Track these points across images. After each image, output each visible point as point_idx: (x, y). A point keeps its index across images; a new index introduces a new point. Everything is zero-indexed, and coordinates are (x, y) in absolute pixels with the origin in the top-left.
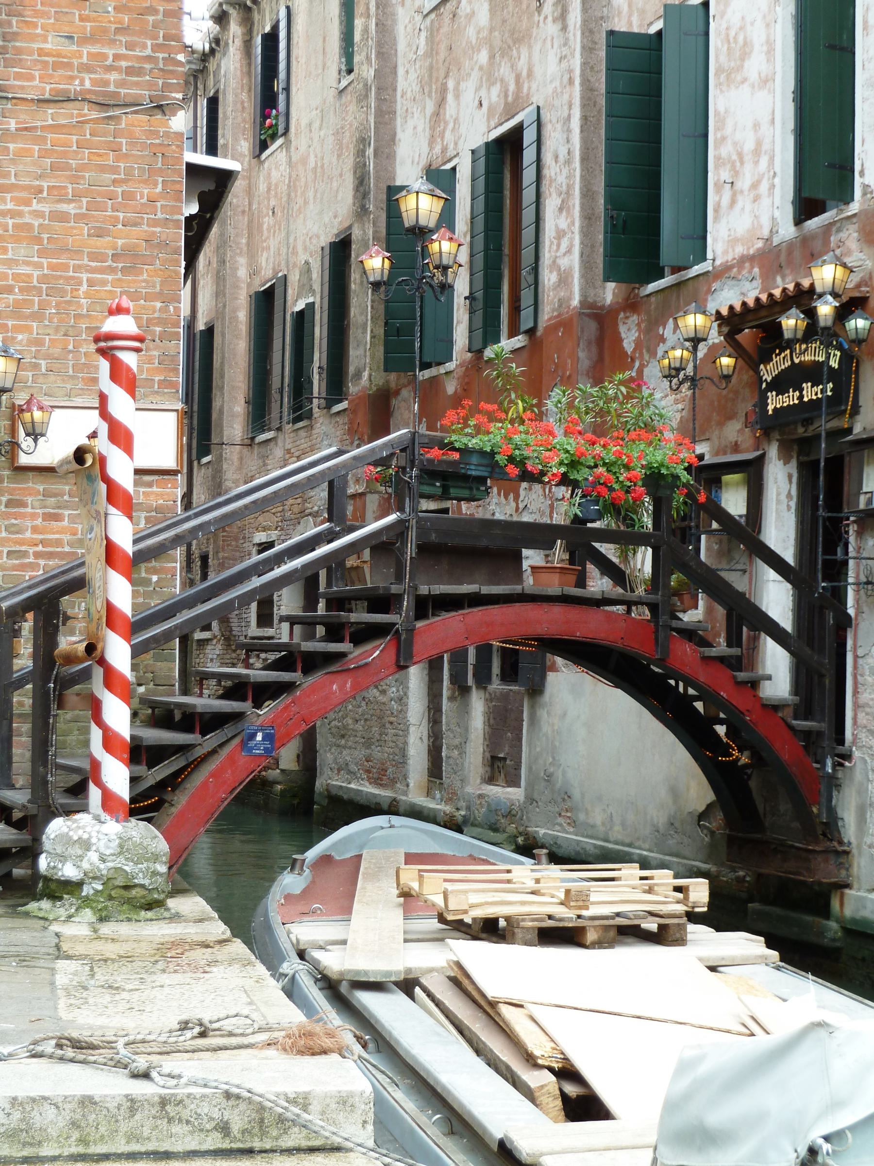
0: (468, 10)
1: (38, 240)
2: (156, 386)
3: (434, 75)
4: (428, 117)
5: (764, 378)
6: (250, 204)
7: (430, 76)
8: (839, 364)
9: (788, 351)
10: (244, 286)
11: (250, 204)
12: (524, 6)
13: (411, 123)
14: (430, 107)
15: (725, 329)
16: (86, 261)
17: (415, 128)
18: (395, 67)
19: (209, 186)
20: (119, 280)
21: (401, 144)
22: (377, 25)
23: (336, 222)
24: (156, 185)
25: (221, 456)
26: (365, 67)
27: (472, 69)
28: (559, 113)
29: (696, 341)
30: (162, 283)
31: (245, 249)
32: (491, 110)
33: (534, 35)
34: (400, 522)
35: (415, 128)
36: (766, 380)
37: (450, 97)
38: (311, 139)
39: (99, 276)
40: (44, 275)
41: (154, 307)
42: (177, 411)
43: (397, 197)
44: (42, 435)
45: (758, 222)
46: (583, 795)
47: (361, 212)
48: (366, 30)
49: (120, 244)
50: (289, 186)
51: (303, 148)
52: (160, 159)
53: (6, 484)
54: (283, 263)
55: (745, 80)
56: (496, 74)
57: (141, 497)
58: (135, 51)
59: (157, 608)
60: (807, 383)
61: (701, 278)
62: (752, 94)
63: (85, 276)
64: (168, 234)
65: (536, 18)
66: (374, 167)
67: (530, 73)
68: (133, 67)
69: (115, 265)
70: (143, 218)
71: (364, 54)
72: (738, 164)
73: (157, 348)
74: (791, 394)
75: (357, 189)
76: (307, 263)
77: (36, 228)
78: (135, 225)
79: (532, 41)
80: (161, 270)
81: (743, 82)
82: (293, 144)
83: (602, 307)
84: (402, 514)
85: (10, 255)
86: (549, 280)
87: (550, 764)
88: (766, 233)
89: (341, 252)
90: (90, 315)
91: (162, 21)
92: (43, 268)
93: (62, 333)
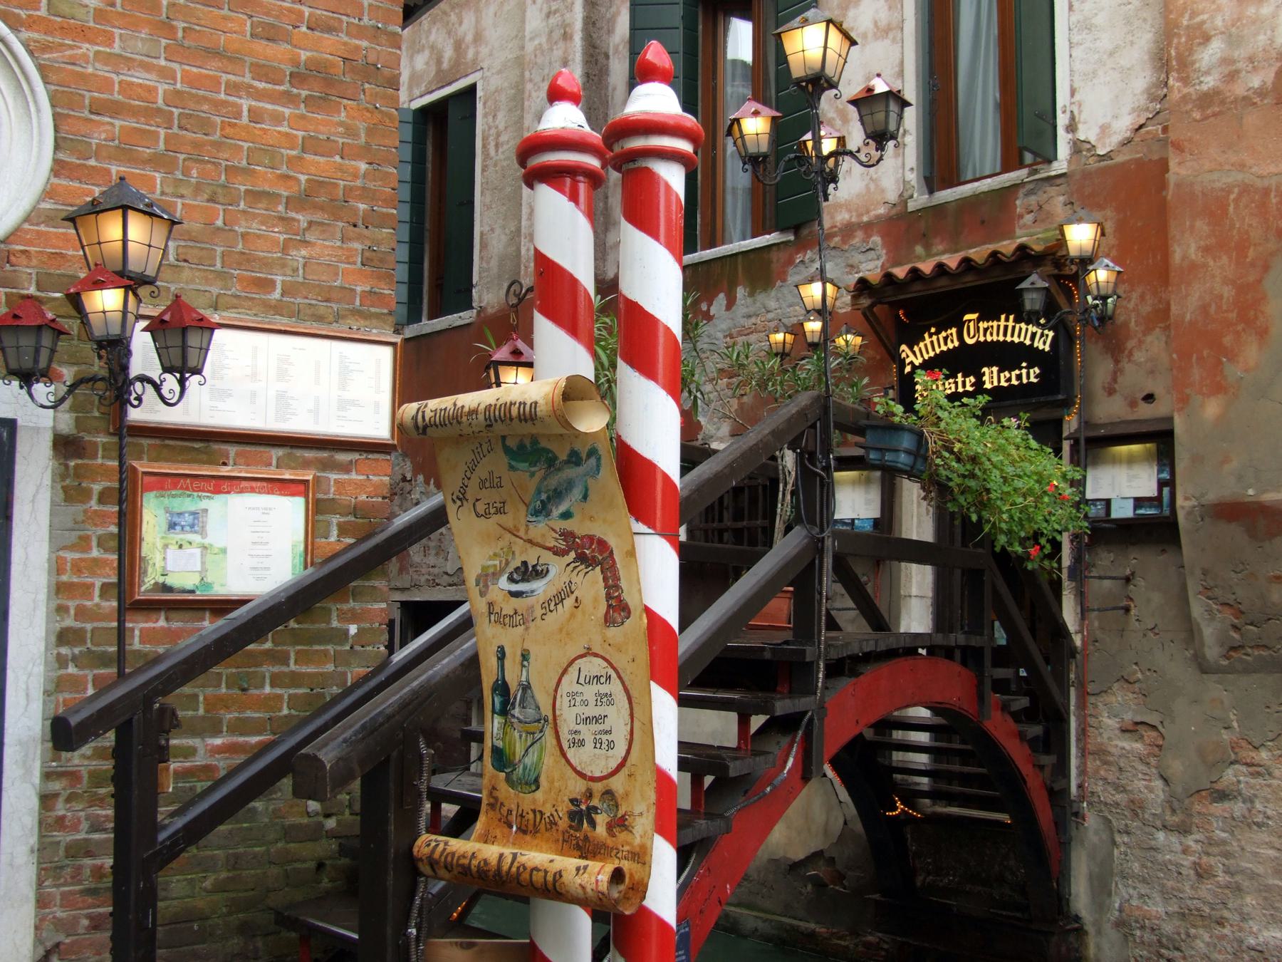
1: (166, 28)
2: (358, 303)
5: (908, 361)
8: (1051, 345)
9: (954, 330)
15: (865, 302)
16: (248, 79)
20: (303, 117)
28: (546, 71)
30: (370, 132)
36: (911, 363)
39: (269, 106)
40: (177, 92)
41: (357, 169)
42: (393, 344)
43: (779, 30)
44: (197, 371)
45: (877, 186)
49: (303, 58)
53: (100, 461)
56: (424, 41)
57: (332, 490)
60: (990, 365)
61: (775, 248)
63: (245, 104)
64: (379, 52)
67: (478, 38)
69: (295, 91)
70: (341, 21)
73: (359, 238)
77: (164, 10)
78: (330, 29)
85: (117, 48)
88: (892, 197)
90: (254, 171)
92: (175, 79)
93: (206, 196)
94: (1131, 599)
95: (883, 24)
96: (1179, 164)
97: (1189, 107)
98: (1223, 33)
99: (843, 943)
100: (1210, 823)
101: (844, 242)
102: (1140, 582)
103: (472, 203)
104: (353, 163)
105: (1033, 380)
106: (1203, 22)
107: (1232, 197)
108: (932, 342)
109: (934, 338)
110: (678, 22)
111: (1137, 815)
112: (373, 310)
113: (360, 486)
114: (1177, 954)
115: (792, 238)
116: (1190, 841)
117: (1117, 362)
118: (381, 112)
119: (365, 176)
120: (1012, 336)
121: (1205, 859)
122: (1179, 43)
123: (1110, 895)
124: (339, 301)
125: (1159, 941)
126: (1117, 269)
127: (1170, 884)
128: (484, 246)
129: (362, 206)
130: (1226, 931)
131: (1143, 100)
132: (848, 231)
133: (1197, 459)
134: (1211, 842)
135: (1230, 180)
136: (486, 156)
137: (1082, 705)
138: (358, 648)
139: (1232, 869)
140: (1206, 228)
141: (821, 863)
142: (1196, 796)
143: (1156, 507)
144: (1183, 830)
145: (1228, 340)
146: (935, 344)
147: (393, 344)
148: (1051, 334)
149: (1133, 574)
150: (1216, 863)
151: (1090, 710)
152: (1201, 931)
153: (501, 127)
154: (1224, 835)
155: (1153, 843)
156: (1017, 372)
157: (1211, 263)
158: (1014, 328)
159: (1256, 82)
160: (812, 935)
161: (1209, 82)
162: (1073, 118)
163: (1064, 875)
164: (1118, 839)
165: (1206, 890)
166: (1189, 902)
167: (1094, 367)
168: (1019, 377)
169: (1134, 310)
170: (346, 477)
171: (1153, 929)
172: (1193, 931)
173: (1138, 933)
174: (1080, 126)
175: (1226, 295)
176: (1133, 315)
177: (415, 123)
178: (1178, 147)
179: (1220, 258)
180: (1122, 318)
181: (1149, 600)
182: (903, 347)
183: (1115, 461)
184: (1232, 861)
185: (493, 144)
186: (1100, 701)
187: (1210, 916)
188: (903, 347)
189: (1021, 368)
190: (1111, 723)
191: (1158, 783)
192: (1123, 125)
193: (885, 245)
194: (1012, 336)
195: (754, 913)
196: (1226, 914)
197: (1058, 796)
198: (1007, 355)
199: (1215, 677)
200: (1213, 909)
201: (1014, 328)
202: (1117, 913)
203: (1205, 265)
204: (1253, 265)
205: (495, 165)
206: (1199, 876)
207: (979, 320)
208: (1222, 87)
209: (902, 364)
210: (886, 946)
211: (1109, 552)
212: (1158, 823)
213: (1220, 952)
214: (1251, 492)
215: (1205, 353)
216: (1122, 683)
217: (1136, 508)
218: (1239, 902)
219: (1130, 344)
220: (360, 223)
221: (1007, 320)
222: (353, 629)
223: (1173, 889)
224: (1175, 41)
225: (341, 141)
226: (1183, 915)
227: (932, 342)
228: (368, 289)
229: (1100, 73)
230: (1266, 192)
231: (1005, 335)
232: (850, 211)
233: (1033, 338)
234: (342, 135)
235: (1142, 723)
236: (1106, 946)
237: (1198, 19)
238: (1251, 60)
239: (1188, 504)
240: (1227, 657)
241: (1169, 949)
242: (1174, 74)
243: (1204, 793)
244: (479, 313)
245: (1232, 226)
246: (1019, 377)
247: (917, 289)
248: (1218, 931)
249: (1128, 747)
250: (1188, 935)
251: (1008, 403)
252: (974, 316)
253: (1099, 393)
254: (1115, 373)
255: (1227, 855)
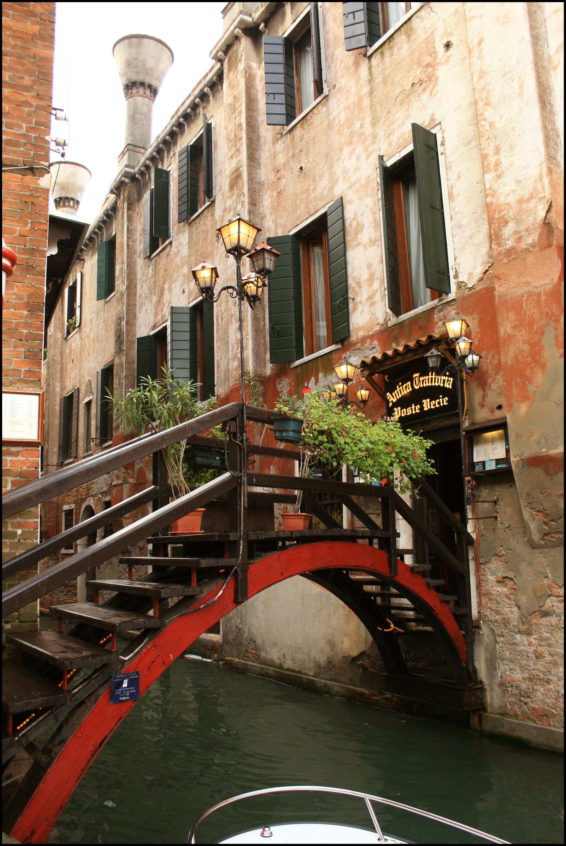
0: (176, 251)
2: (22, 376)
3: (157, 284)
4: (154, 304)
5: (390, 400)
6: (62, 360)
7: (155, 285)
8: (452, 386)
9: (409, 383)
10: (58, 395)
11: (62, 360)
12: (209, 241)
13: (144, 309)
14: (155, 299)
15: (366, 373)
17: (146, 310)
18: (136, 285)
19: (66, 236)
21: (139, 319)
22: (127, 266)
23: (104, 360)
24: (26, 224)
25: (47, 471)
26: (121, 286)
27: (179, 277)
29: (346, 380)
31: (59, 379)
32: (190, 293)
33: (215, 253)
34: (232, 478)
35: (146, 310)
36: (392, 401)
37: (166, 292)
38: (92, 326)
42: (39, 394)
45: (375, 317)
46: (263, 642)
47: (119, 351)
48: (122, 269)
50: (80, 349)
51: (88, 331)
52: (30, 206)
54: (77, 383)
55: (359, 244)
57: (9, 465)
58: (13, 129)
59: (21, 558)
60: (426, 399)
61: (334, 352)
62: (365, 250)
65: (216, 245)
66: (126, 330)
68: (11, 140)
71: (120, 280)
72: (357, 288)
73: (23, 346)
74: (413, 407)
75: (117, 341)
76: (89, 381)
79: (214, 256)
80: (28, 286)
81: (357, 246)
82: (83, 330)
83: (265, 377)
84: (234, 472)
86: (232, 365)
87: (240, 623)
88: (381, 321)
89: (107, 373)
91: (34, 112)
94: (498, 513)
95: (373, 239)
96: (500, 286)
97: (502, 257)
98: (513, 219)
99: (376, 698)
100: (540, 629)
101: (362, 345)
102: (501, 503)
103: (213, 347)
104: (21, 311)
105: (445, 404)
106: (505, 215)
107: (524, 299)
108: (400, 390)
109: (401, 387)
110: (289, 251)
111: (506, 626)
112: (30, 379)
113: (23, 463)
114: (529, 700)
115: (340, 346)
116: (532, 639)
117: (484, 390)
118: (36, 287)
119: (26, 317)
120: (435, 382)
121: (539, 648)
122: (495, 227)
123: (495, 669)
124: (12, 376)
125: (520, 693)
126: (470, 341)
127: (523, 662)
128: (218, 367)
129: (25, 331)
130: (551, 687)
131: (486, 258)
132: (364, 340)
133: (518, 436)
134: (541, 639)
135: (523, 291)
136: (218, 325)
137: (478, 570)
138: (22, 541)
139: (552, 653)
140: (514, 317)
141: (366, 657)
142: (533, 615)
143: (505, 463)
144: (528, 633)
145: (528, 372)
146: (403, 390)
147: (39, 394)
148: (452, 379)
149: (498, 499)
150: (544, 650)
151: (482, 572)
152: (539, 687)
153: (223, 310)
154: (548, 635)
155: (515, 641)
156: (438, 400)
157: (518, 334)
158: (435, 378)
159: (530, 240)
160: (362, 694)
161: (510, 244)
162: (456, 272)
163: (470, 658)
164: (498, 639)
165: (540, 665)
166: (533, 672)
167: (474, 395)
168: (439, 403)
169: (490, 363)
170: (16, 458)
171: (517, 687)
172: (535, 687)
173: (510, 689)
174: (460, 275)
175: (525, 349)
176: (490, 366)
177: (191, 313)
178: (498, 277)
179: (521, 331)
180: (485, 368)
181: (505, 513)
182: (388, 394)
183: (486, 441)
184: (552, 649)
185: (220, 318)
186: (486, 567)
187: (543, 679)
188: (388, 394)
189: (439, 398)
190: (492, 578)
191: (515, 609)
192: (478, 272)
193: (379, 345)
194: (435, 382)
195: (338, 684)
196: (551, 677)
197: (463, 617)
198: (433, 392)
199: (538, 551)
200: (544, 675)
201: (435, 378)
202: (500, 679)
203: (515, 335)
204: (536, 332)
205: (222, 328)
206: (537, 657)
207: (420, 376)
208: (515, 245)
209: (388, 402)
210: (395, 699)
211: (486, 489)
212: (516, 630)
213: (549, 698)
214: (544, 450)
215: (518, 380)
216: (496, 557)
217: (497, 464)
218: (556, 670)
219: (490, 381)
220: (24, 339)
221: (432, 375)
222: (19, 532)
223: (525, 665)
224: (493, 226)
225: (14, 302)
226: (531, 678)
227: (400, 390)
228: (27, 369)
229: (467, 248)
230: (539, 294)
231: (432, 383)
232: (364, 330)
233: (444, 383)
234: (15, 299)
235: (506, 577)
236: (495, 696)
237: (502, 214)
238: (527, 230)
239: (516, 459)
240: (543, 539)
241: (525, 697)
242: (494, 242)
243: (537, 613)
244: (217, 398)
245: (525, 314)
246: (439, 403)
247: (388, 365)
248: (548, 687)
249: (500, 590)
250: (533, 690)
251: (435, 416)
252: (417, 375)
253: (477, 407)
254: (484, 396)
255: (550, 645)
